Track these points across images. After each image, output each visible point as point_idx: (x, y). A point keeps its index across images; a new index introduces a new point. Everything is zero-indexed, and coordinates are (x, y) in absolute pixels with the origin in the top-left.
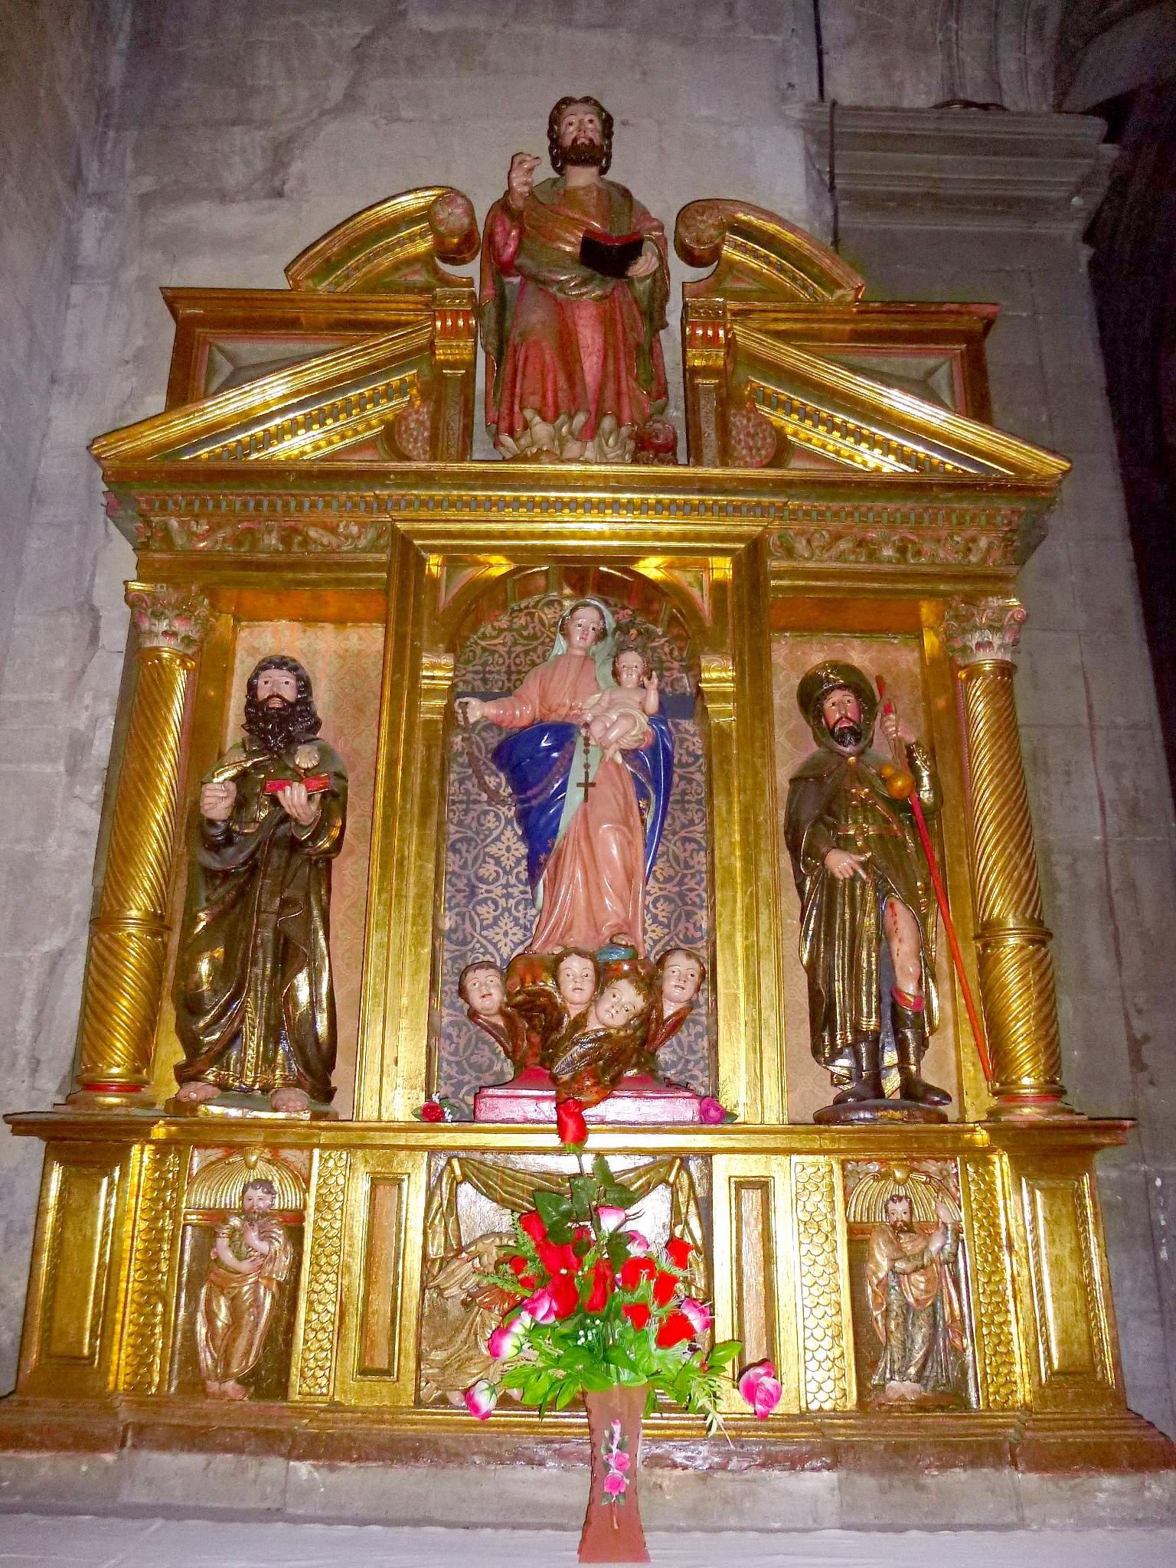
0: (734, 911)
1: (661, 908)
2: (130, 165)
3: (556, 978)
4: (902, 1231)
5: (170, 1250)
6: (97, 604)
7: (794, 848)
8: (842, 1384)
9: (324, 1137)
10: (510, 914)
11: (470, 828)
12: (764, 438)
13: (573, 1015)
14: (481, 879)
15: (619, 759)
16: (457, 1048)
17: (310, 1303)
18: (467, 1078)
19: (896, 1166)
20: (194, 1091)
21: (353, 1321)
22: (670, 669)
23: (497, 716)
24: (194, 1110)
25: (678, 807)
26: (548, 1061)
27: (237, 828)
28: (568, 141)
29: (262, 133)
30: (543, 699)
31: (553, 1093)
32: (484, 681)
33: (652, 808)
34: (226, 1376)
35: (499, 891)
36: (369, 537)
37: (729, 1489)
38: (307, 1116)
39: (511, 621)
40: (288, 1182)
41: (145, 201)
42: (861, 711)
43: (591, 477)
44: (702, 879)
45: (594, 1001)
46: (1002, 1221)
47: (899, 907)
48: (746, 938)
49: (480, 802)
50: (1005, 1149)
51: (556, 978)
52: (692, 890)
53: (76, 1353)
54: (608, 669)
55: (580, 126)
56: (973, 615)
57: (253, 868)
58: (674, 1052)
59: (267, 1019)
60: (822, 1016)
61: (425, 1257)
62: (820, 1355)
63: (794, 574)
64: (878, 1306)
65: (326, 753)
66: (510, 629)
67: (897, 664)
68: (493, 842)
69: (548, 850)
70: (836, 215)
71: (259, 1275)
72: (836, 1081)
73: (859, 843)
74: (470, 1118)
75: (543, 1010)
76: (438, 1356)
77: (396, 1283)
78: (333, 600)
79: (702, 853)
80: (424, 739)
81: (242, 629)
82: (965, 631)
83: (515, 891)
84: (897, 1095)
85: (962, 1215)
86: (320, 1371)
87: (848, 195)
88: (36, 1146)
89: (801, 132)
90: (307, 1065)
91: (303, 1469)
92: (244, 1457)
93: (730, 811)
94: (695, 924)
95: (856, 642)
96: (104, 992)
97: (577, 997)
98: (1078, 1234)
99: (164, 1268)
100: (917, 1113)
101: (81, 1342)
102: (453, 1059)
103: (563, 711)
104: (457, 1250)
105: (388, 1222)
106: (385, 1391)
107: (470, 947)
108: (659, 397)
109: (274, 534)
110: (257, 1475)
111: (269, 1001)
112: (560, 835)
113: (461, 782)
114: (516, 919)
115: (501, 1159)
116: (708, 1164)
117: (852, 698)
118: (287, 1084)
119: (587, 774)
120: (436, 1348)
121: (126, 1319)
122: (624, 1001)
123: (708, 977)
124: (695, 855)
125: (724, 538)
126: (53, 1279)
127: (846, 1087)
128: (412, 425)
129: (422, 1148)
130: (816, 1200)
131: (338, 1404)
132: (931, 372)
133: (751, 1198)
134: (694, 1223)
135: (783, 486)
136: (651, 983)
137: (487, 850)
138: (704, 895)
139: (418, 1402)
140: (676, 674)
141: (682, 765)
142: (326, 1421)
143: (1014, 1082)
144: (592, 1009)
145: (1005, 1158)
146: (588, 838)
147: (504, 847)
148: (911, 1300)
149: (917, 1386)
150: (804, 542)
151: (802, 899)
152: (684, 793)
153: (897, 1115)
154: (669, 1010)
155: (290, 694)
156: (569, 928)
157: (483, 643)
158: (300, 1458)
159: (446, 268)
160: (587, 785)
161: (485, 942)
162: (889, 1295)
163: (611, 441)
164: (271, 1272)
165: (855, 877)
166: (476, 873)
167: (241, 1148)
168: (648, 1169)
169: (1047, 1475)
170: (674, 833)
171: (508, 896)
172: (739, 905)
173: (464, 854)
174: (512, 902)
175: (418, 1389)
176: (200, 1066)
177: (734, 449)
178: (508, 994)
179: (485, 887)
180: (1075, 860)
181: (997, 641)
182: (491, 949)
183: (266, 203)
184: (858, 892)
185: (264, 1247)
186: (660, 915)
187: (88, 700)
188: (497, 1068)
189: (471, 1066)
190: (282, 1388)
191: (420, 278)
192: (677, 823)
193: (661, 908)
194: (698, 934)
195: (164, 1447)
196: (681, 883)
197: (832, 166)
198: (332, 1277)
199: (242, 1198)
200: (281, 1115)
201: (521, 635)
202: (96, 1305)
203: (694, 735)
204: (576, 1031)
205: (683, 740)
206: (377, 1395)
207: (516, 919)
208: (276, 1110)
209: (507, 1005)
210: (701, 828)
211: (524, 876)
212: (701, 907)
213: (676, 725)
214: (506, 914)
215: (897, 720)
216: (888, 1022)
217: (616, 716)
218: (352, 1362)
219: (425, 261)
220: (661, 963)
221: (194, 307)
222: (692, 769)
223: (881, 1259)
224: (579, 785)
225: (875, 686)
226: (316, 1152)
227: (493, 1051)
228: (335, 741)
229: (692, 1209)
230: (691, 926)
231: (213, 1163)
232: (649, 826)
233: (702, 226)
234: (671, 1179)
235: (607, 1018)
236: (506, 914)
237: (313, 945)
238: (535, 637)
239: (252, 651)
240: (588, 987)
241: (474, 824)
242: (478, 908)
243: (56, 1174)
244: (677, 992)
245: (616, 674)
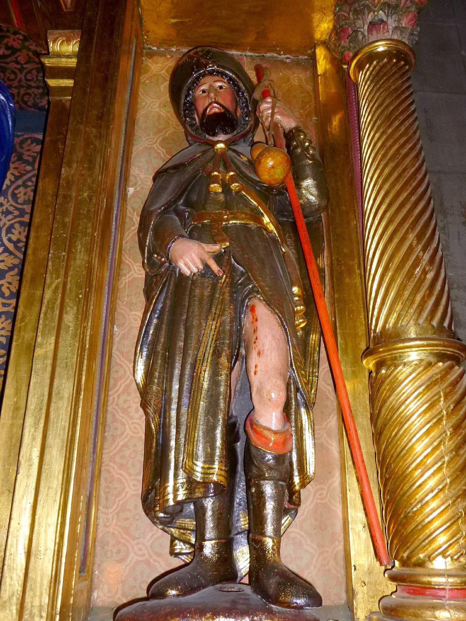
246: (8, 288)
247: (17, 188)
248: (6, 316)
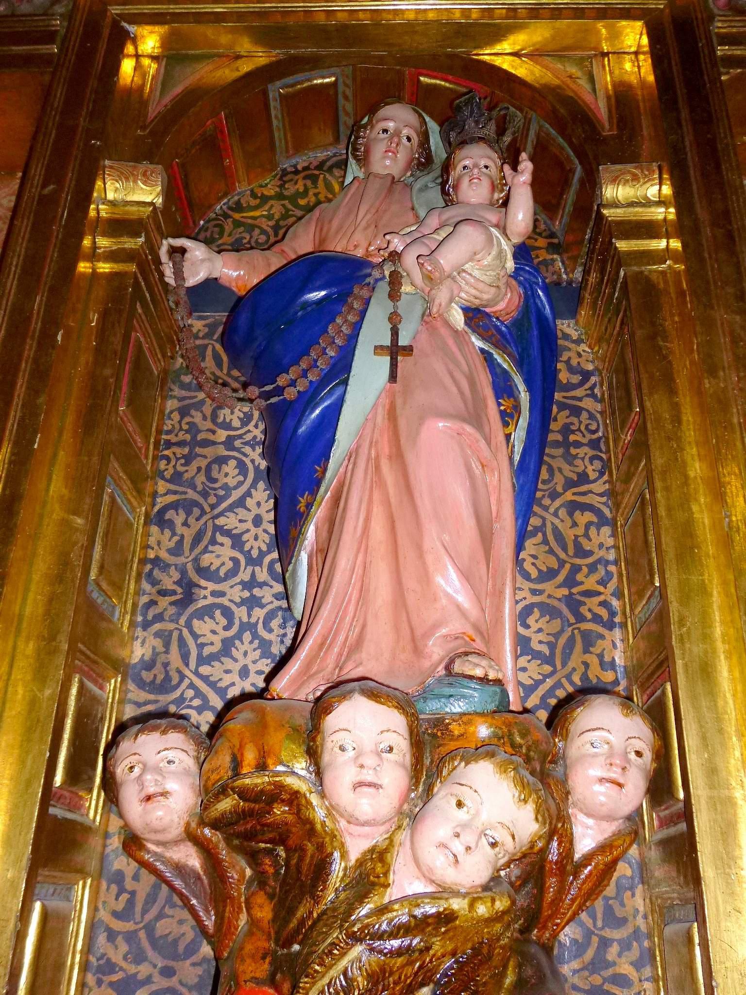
1: (535, 627)
3: (313, 754)
10: (255, 636)
11: (194, 487)
13: (354, 855)
14: (204, 572)
16: (131, 903)
18: (144, 970)
25: (560, 451)
35: (237, 593)
39: (281, 186)
44: (609, 575)
45: (410, 815)
49: (214, 443)
51: (313, 754)
52: (589, 594)
68: (230, 508)
94: (601, 656)
97: (366, 805)
102: (117, 925)
107: (177, 694)
113: (184, 412)
124: (593, 531)
137: (221, 521)
138: (615, 603)
144: (403, 836)
146: (398, 456)
147: (250, 517)
152: (566, 430)
156: (358, 644)
157: (237, 216)
160: (395, 351)
166: (196, 560)
170: (554, 495)
171: (252, 603)
173: (180, 529)
179: (211, 586)
193: (535, 627)
196: (571, 582)
203: (578, 342)
204: (361, 898)
209: (202, 823)
210: (600, 487)
212: (610, 626)
214: (247, 636)
222: (579, 393)
230: (594, 661)
235: (440, 864)
240: (393, 777)
241: (201, 479)
242: (196, 623)
244: (602, 794)
246: (533, 564)
247: (240, 484)
248: (540, 611)
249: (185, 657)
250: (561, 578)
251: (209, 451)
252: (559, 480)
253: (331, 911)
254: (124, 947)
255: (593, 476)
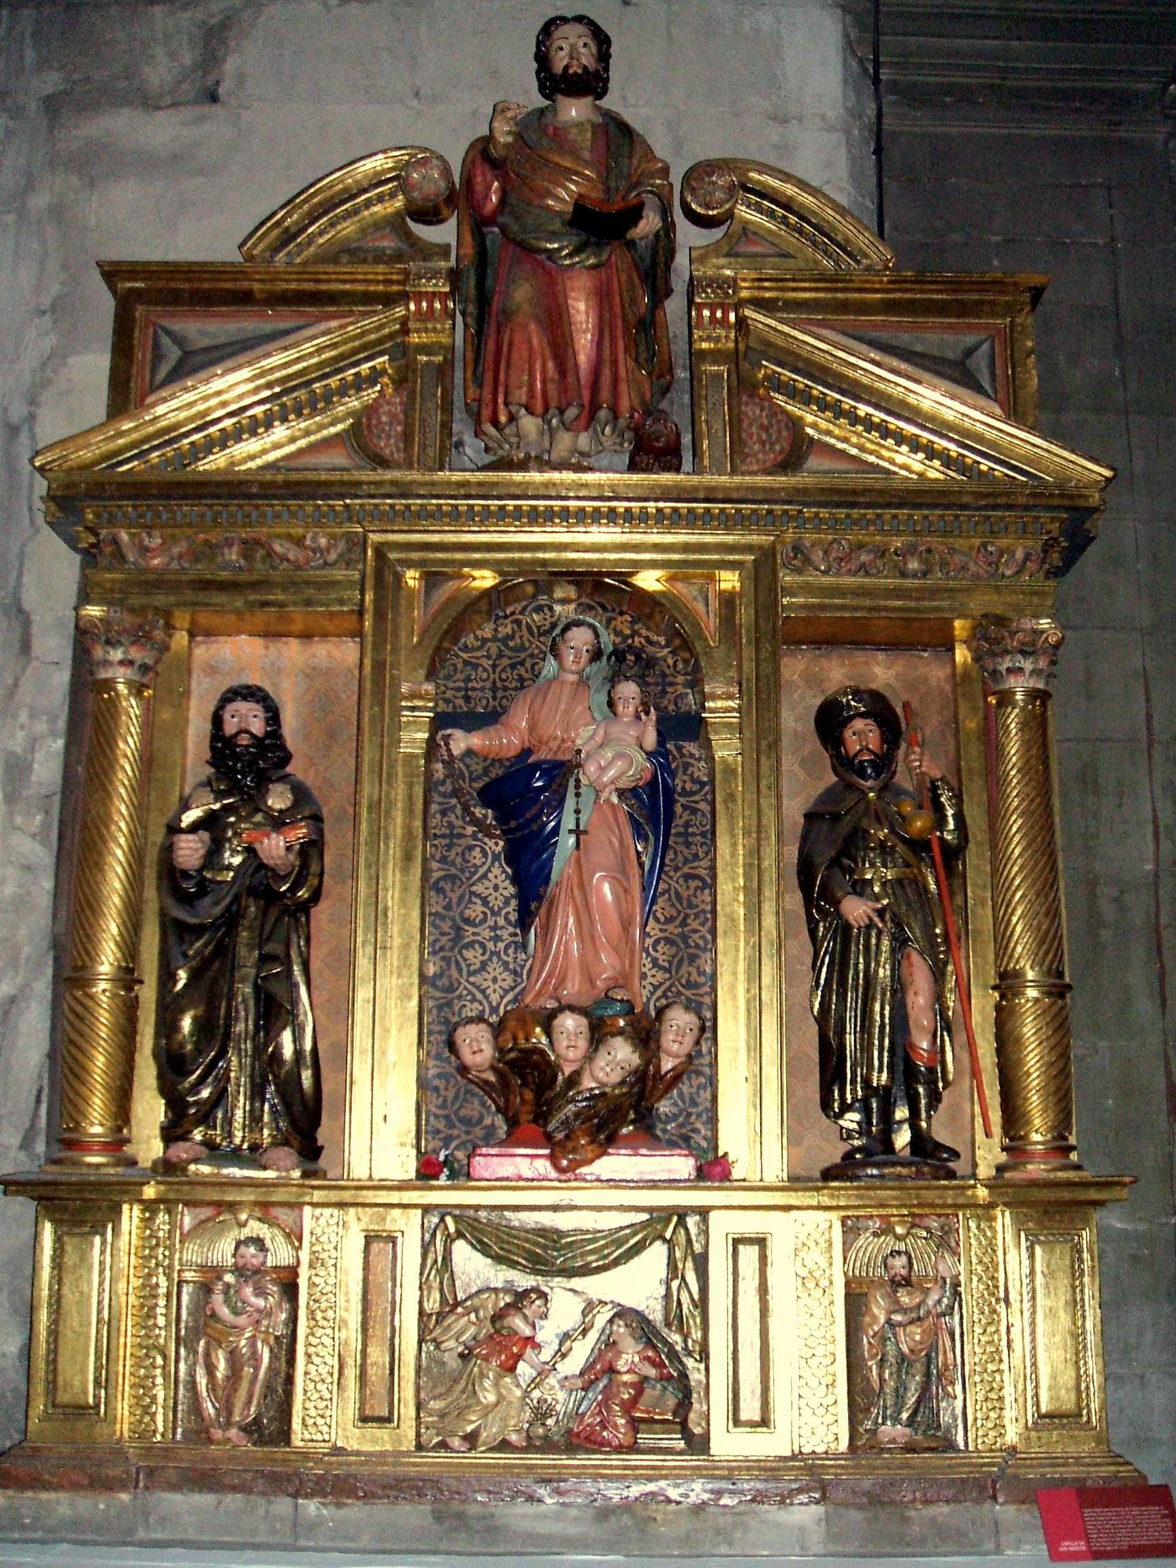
0: (736, 961)
2: (30, 55)
4: (900, 1285)
5: (166, 1306)
6: (27, 606)
7: (806, 885)
8: (834, 1429)
9: (318, 1196)
12: (779, 431)
14: (467, 921)
15: (615, 800)
16: (445, 1101)
17: (308, 1355)
18: (455, 1132)
19: (898, 1223)
20: (181, 1151)
21: (351, 1373)
22: (672, 684)
23: (484, 746)
24: (184, 1170)
25: (681, 840)
26: (541, 1117)
27: (209, 875)
28: (558, 67)
29: (188, 15)
30: (532, 727)
31: (547, 1152)
32: (467, 699)
33: (651, 849)
34: (229, 1424)
35: (487, 934)
36: (339, 550)
37: (721, 1520)
38: (296, 1174)
40: (280, 1239)
41: (53, 106)
42: (884, 740)
43: (585, 486)
45: (589, 1057)
46: (1001, 1276)
47: (915, 958)
48: (748, 991)
49: (464, 836)
50: (1005, 1204)
51: (548, 1032)
52: (695, 931)
53: (82, 1402)
54: (605, 699)
55: (572, 50)
56: (1003, 638)
57: (231, 919)
58: (675, 1104)
59: (252, 1077)
60: (831, 1067)
61: (421, 1312)
62: (815, 1403)
63: (808, 589)
64: (873, 1357)
65: (301, 794)
66: (495, 639)
67: (926, 680)
69: (540, 898)
70: (879, 116)
71: (256, 1329)
72: (847, 1135)
73: (876, 889)
74: (461, 1174)
75: (536, 1066)
76: (436, 1405)
77: (393, 1336)
78: (299, 618)
79: (707, 891)
80: (405, 776)
81: (198, 643)
82: (994, 655)
83: (505, 934)
84: (908, 1151)
85: (961, 1268)
86: (325, 1418)
87: (894, 87)
88: (23, 1207)
89: (839, 12)
90: (293, 1122)
91: (311, 1507)
92: (253, 1497)
93: (734, 855)
95: (881, 656)
96: (79, 1048)
97: (571, 1054)
98: (1074, 1288)
99: (161, 1321)
100: (926, 1169)
101: (85, 1393)
102: (440, 1112)
103: (554, 745)
104: (451, 1305)
105: (381, 1276)
106: (386, 1438)
108: (661, 376)
109: (235, 549)
110: (267, 1512)
111: (254, 1057)
112: (552, 884)
113: (444, 813)
114: (506, 964)
115: (494, 1215)
116: (705, 1220)
117: (874, 728)
118: (275, 1144)
119: (578, 820)
120: (434, 1398)
121: (125, 1368)
122: (620, 1056)
123: (708, 1029)
125: (730, 548)
126: (54, 1334)
127: (857, 1143)
128: (384, 419)
129: (415, 1206)
130: (815, 1256)
131: (342, 1448)
132: (970, 352)
133: (749, 1254)
134: (691, 1277)
135: (800, 496)
136: (646, 1036)
137: (474, 888)
139: (419, 1447)
140: (680, 690)
141: (685, 793)
142: (331, 1463)
143: (1021, 1138)
145: (1007, 1214)
146: (582, 886)
147: (491, 885)
148: (905, 1349)
149: (908, 1430)
150: (820, 553)
151: (814, 946)
152: (687, 824)
153: (904, 1171)
154: (667, 1064)
155: (258, 727)
156: (562, 981)
157: (464, 655)
158: (306, 1496)
159: (419, 230)
160: (577, 832)
161: (474, 990)
162: (885, 1346)
163: (608, 430)
164: (268, 1327)
165: (870, 926)
166: (462, 914)
167: (233, 1207)
168: (644, 1225)
169: (1023, 1507)
170: (677, 869)
171: (497, 939)
172: (741, 955)
173: (450, 894)
174: (501, 945)
175: (418, 1435)
176: (187, 1126)
177: (745, 444)
178: (501, 1050)
179: (472, 930)
180: (1122, 893)
181: (1028, 665)
182: (479, 996)
183: (198, 111)
184: (874, 941)
185: (261, 1303)
186: (661, 958)
187: (23, 717)
188: (488, 1121)
189: (462, 1120)
190: (285, 1435)
191: (389, 243)
192: (680, 858)
194: (702, 980)
195: (174, 1487)
196: (684, 923)
197: (876, 57)
198: (329, 1331)
199: (234, 1256)
200: (270, 1174)
201: (507, 646)
202: (98, 1358)
203: (699, 760)
205: (686, 766)
206: (377, 1440)
207: (506, 964)
208: (265, 1168)
211: (513, 917)
213: (679, 749)
214: (495, 959)
215: (922, 754)
216: (900, 1076)
217: (612, 751)
218: (351, 1410)
219: (396, 224)
220: (660, 1012)
221: (136, 280)
222: (696, 798)
223: (879, 1310)
224: (570, 831)
225: (899, 711)
226: (307, 1209)
227: (483, 1104)
228: (306, 771)
229: (690, 1264)
230: (693, 970)
231: (202, 1222)
232: (647, 868)
233: (710, 188)
234: (668, 1235)
236: (495, 959)
237: (295, 1001)
238: (522, 648)
239: (212, 670)
240: (582, 1043)
241: (459, 860)
243: (48, 1230)
245: (611, 704)
249: (460, 971)
250: (678, 922)
251: (463, 841)
252: (680, 858)
253: (558, 1095)
254: (443, 1122)
255: (701, 855)
